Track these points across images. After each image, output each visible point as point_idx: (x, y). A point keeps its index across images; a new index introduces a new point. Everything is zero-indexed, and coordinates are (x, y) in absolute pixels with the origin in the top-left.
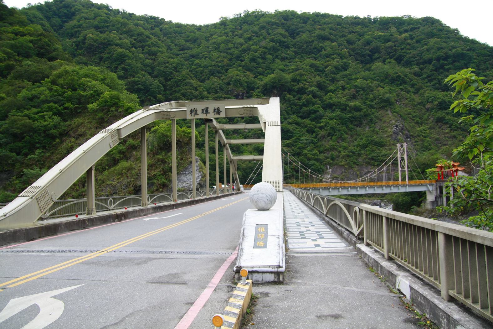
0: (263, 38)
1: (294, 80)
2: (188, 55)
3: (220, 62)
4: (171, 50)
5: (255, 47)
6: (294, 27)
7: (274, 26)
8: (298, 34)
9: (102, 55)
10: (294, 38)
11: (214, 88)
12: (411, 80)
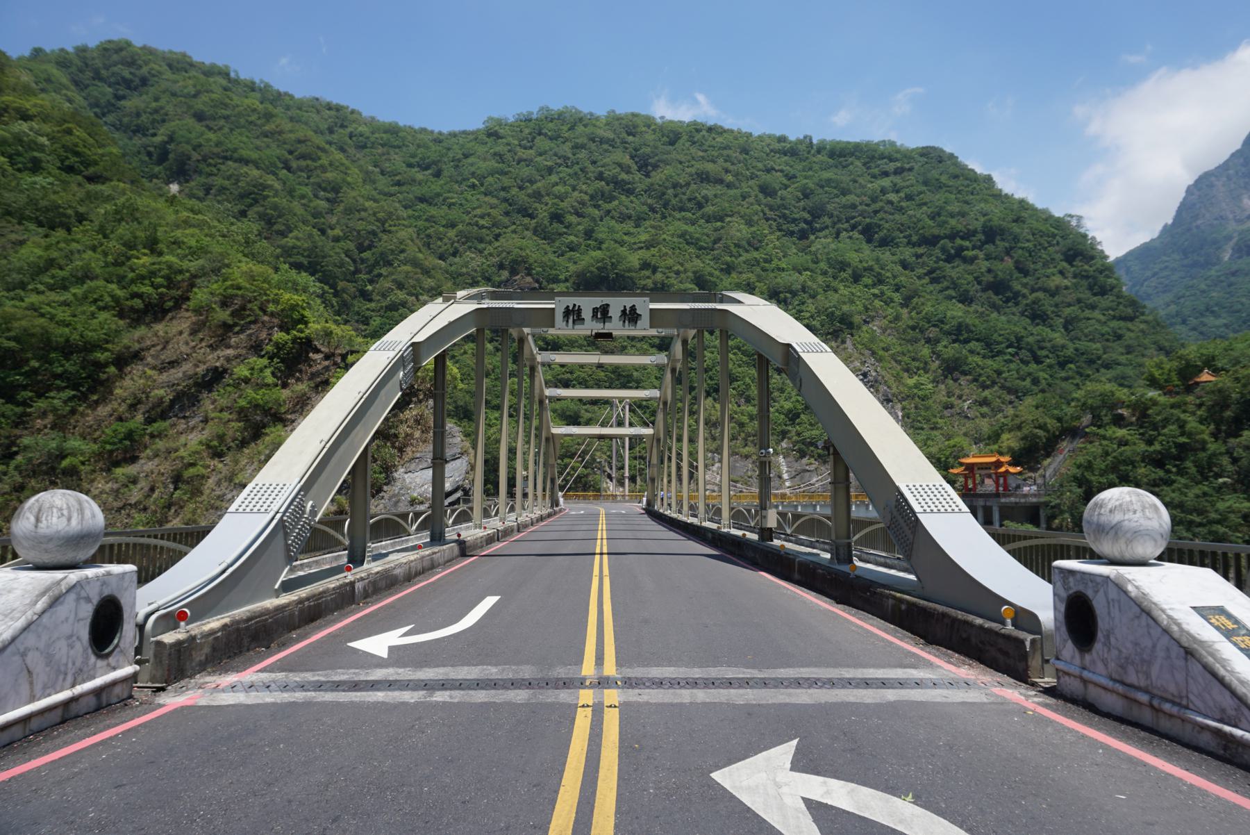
0: (581, 170)
1: (645, 265)
2: (411, 196)
3: (482, 217)
4: (374, 182)
5: (560, 189)
6: (648, 150)
7: (605, 146)
8: (655, 167)
9: (210, 180)
10: (647, 175)
11: (468, 274)
12: (895, 277)
